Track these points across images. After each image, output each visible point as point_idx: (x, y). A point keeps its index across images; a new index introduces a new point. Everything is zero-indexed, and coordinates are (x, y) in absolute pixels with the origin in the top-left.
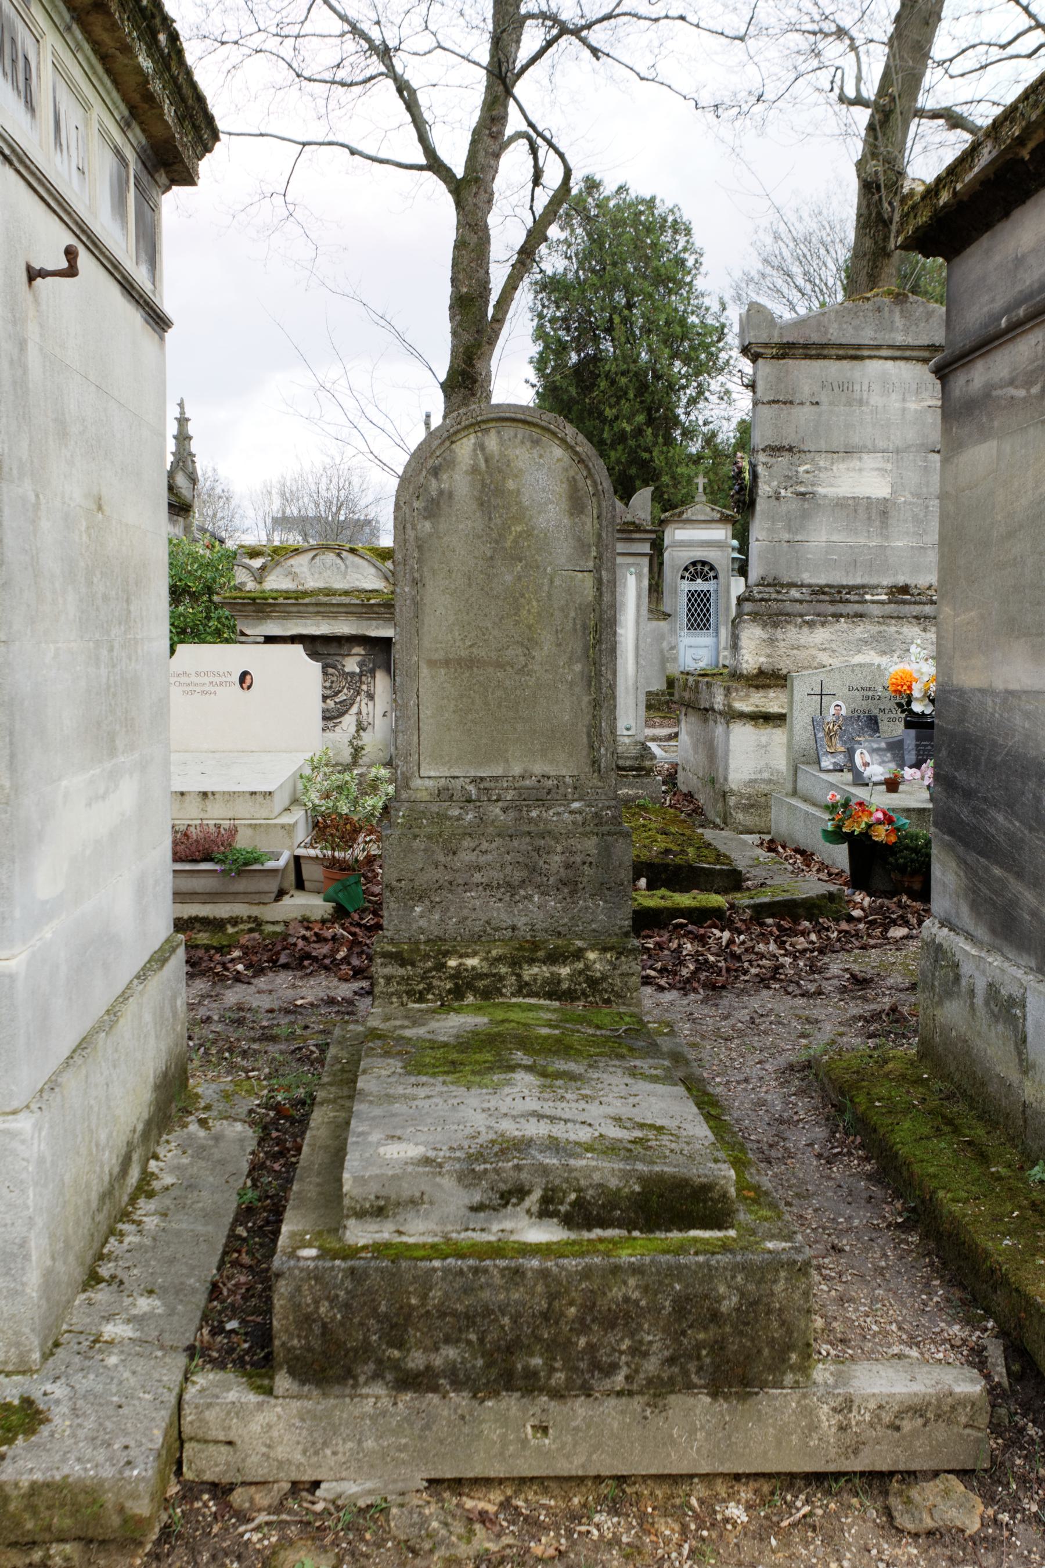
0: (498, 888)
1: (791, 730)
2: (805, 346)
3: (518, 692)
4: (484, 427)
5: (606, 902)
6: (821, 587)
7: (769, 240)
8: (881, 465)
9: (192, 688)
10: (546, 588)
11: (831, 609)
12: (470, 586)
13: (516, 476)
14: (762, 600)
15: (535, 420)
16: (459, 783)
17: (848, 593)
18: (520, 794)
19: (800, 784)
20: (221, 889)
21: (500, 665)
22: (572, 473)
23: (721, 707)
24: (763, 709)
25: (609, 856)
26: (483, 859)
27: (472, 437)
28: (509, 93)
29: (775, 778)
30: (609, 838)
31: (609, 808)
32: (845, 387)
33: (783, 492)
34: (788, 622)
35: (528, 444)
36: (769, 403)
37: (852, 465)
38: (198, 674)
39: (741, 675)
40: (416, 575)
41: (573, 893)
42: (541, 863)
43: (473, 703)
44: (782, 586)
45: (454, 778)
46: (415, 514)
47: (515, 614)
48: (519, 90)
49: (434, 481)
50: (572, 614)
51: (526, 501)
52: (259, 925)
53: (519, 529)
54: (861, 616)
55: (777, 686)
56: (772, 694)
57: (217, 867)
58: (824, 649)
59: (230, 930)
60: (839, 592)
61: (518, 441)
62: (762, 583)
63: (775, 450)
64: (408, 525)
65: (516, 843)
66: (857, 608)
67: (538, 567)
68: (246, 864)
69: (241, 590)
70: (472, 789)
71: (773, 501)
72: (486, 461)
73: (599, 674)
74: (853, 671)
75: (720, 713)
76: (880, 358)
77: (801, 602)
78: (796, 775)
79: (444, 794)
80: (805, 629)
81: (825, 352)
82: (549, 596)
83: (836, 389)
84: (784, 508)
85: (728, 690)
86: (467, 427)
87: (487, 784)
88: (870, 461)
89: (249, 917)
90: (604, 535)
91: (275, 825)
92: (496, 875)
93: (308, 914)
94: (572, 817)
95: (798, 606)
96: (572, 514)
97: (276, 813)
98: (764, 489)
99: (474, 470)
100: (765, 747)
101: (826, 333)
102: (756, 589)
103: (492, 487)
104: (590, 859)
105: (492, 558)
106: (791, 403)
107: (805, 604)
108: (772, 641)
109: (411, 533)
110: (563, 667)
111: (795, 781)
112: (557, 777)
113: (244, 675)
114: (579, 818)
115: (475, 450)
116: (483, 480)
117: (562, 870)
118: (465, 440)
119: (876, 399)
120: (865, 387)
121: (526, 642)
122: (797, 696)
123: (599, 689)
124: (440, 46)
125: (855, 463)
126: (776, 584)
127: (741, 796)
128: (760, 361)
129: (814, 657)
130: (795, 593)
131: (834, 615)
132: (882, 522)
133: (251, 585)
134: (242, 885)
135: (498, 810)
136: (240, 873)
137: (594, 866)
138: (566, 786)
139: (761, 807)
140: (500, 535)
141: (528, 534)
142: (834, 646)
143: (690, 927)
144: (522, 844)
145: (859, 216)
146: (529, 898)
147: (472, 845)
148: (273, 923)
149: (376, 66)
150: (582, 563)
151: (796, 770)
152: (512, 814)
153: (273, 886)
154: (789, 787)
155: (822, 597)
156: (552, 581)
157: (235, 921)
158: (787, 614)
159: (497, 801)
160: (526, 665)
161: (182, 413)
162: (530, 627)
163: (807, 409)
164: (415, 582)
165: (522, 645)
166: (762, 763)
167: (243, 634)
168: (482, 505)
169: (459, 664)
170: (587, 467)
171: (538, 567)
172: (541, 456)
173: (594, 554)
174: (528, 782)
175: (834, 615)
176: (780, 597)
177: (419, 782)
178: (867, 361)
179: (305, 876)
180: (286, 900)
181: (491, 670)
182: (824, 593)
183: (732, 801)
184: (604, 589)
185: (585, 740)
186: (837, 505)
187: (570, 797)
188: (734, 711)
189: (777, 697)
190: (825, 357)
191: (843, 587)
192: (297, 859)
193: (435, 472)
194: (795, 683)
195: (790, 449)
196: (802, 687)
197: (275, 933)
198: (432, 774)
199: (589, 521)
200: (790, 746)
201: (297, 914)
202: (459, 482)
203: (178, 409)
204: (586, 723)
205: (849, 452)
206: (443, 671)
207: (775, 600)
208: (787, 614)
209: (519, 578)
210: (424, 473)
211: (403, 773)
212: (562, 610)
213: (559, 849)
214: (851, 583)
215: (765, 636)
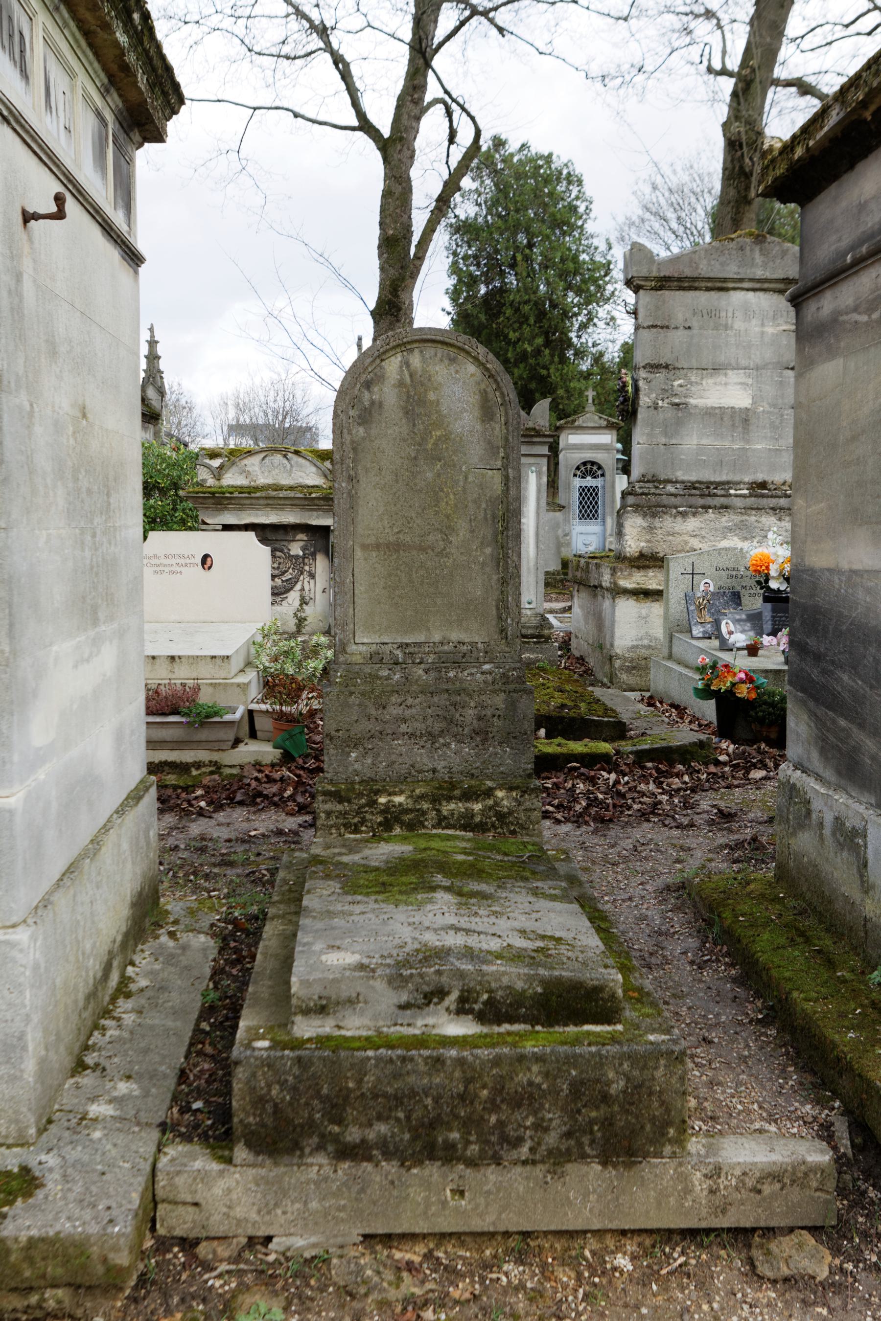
0: (421, 737)
2: (679, 279)
3: (438, 572)
4: (409, 347)
5: (512, 748)
6: (693, 483)
7: (648, 189)
8: (744, 380)
9: (161, 568)
10: (461, 484)
11: (701, 501)
12: (397, 481)
13: (436, 389)
14: (643, 494)
15: (452, 341)
16: (388, 648)
17: (716, 488)
18: (440, 658)
19: (675, 649)
20: (187, 738)
21: (422, 549)
22: (483, 386)
23: (608, 585)
24: (644, 586)
26: (408, 712)
27: (399, 356)
28: (428, 65)
29: (653, 644)
31: (514, 669)
32: (712, 314)
33: (660, 403)
35: (446, 362)
36: (649, 327)
37: (718, 380)
38: (166, 557)
39: (625, 558)
40: (352, 473)
41: (484, 740)
42: (457, 716)
43: (400, 581)
44: (660, 482)
45: (383, 644)
47: (436, 506)
49: (366, 393)
53: (438, 433)
54: (727, 507)
55: (655, 567)
56: (651, 573)
57: (183, 720)
58: (695, 536)
59: (194, 772)
60: (708, 488)
61: (437, 359)
62: (643, 480)
63: (654, 367)
64: (345, 431)
65: (436, 699)
66: (723, 500)
67: (454, 466)
68: (207, 717)
70: (399, 654)
72: (411, 376)
73: (506, 556)
74: (719, 554)
75: (607, 590)
76: (742, 289)
77: (675, 495)
78: (671, 641)
79: (376, 658)
80: (679, 519)
81: (696, 284)
82: (464, 490)
85: (614, 571)
86: (394, 348)
87: (411, 649)
88: (734, 377)
89: (210, 762)
91: (232, 684)
92: (419, 726)
93: (260, 758)
95: (673, 499)
96: (483, 421)
97: (233, 674)
98: (644, 400)
99: (401, 384)
100: (644, 619)
101: (697, 268)
102: (637, 485)
104: (498, 713)
105: (415, 458)
106: (667, 327)
107: (679, 498)
108: (651, 529)
109: (347, 438)
110: (476, 550)
111: (671, 647)
112: (471, 643)
113: (205, 557)
114: (489, 678)
115: (401, 367)
116: (408, 392)
117: (475, 721)
119: (739, 325)
120: (730, 314)
121: (444, 529)
122: (672, 576)
123: (506, 569)
125: (721, 379)
126: (654, 480)
127: (625, 659)
128: (641, 292)
129: (686, 543)
130: (670, 488)
131: (703, 507)
132: (744, 428)
133: (211, 482)
134: (204, 734)
135: (421, 672)
136: (202, 724)
137: (502, 718)
138: (479, 651)
139: (641, 669)
140: (422, 439)
141: (446, 438)
142: (703, 533)
143: (582, 770)
144: (441, 700)
145: (725, 169)
146: (447, 745)
148: (230, 767)
149: (316, 42)
152: (433, 675)
153: (231, 735)
154: (665, 651)
155: (694, 492)
156: (466, 478)
157: (198, 765)
158: (664, 506)
159: (420, 663)
160: (445, 549)
161: (152, 336)
162: (448, 516)
163: (681, 332)
164: (351, 479)
165: (441, 532)
166: (643, 632)
167: (204, 523)
168: (407, 413)
170: (496, 381)
172: (457, 372)
173: (502, 455)
174: (446, 648)
175: (703, 507)
176: (658, 491)
177: (354, 647)
178: (732, 292)
180: (242, 747)
181: (414, 552)
182: (695, 488)
183: (617, 663)
184: (511, 484)
185: (494, 612)
186: (706, 413)
187: (481, 660)
189: (655, 576)
190: (696, 289)
191: (712, 483)
192: (251, 713)
193: (368, 385)
194: (671, 564)
195: (667, 367)
196: (676, 567)
197: (231, 775)
198: (365, 641)
201: (251, 760)
202: (388, 394)
204: (495, 597)
205: (717, 369)
206: (374, 554)
207: (653, 494)
208: (664, 506)
209: (439, 475)
210: (358, 386)
211: (340, 640)
213: (473, 704)
215: (645, 525)
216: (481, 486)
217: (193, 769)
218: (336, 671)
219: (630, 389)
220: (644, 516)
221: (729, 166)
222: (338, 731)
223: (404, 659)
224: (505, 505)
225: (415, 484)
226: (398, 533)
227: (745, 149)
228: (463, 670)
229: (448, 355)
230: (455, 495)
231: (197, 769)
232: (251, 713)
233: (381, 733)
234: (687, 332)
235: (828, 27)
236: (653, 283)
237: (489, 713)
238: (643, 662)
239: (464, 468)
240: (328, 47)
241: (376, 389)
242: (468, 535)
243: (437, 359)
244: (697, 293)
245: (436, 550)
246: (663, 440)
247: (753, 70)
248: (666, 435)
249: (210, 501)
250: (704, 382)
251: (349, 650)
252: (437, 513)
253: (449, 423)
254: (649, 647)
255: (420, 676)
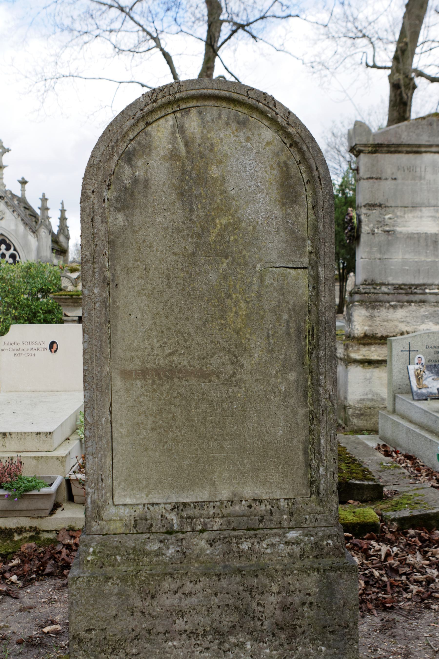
0: (204, 636)
1: (390, 372)
2: (388, 146)
3: (225, 405)
4: (183, 106)
5: (329, 647)
6: (400, 285)
7: (330, 135)
8: (433, 214)
9: (20, 352)
10: (255, 287)
11: (406, 298)
12: (169, 285)
13: (221, 162)
14: (365, 293)
15: (241, 97)
16: (160, 510)
17: (416, 289)
18: (229, 523)
19: (398, 407)
20: (10, 508)
21: (204, 375)
22: (283, 158)
23: (342, 356)
24: (368, 358)
25: (332, 594)
26: (186, 603)
27: (170, 118)
28: (215, 54)
29: (375, 398)
30: (332, 574)
31: (330, 537)
32: (411, 169)
33: (376, 230)
34: (381, 306)
35: (234, 126)
36: (368, 179)
37: (416, 214)
38: (24, 343)
39: (354, 338)
40: (108, 274)
41: (291, 638)
42: (254, 604)
43: (174, 419)
44: (377, 285)
45: (153, 504)
46: (106, 205)
47: (221, 317)
48: (219, 53)
49: (127, 168)
50: (285, 316)
51: (231, 188)
52: (38, 533)
53: (224, 221)
54: (424, 302)
55: (376, 344)
56: (373, 348)
57: (6, 493)
58: (403, 322)
59: (17, 537)
60: (410, 288)
61: (222, 122)
62: (365, 283)
63: (371, 206)
64: (98, 218)
65: (224, 583)
66: (421, 297)
67: (246, 264)
68: (26, 491)
69: (65, 291)
70: (173, 517)
71: (371, 236)
72: (187, 145)
73: (316, 384)
74: (428, 336)
75: (341, 359)
76: (431, 152)
77: (388, 294)
78: (394, 400)
79: (141, 525)
80: (391, 310)
81: (400, 149)
82: (259, 295)
83: (406, 171)
84: (377, 239)
85: (347, 347)
86: (163, 106)
87: (190, 512)
88: (426, 212)
89: (31, 527)
90: (321, 227)
91: (52, 457)
92: (202, 621)
93: (73, 524)
94: (288, 549)
95: (386, 297)
96: (284, 204)
97: (56, 445)
98: (365, 229)
99: (173, 155)
100: (369, 380)
101: (400, 138)
102: (361, 287)
103: (194, 174)
104: (310, 599)
105: (194, 254)
106: (380, 179)
107: (391, 296)
108: (372, 317)
109: (101, 228)
110: (276, 376)
111: (394, 404)
112: (270, 501)
113: (53, 343)
114: (296, 549)
115: (173, 133)
116: (183, 167)
117: (278, 612)
118: (162, 121)
119: (429, 176)
120: (423, 169)
121: (233, 349)
122: (394, 352)
123: (317, 401)
124: (182, 31)
125: (418, 213)
126: (373, 284)
127: (356, 409)
128: (362, 155)
129: (396, 326)
130: (384, 289)
131: (408, 302)
132: (434, 247)
133: (70, 288)
134: (24, 505)
135: (203, 543)
136: (22, 497)
137: (315, 607)
138: (281, 512)
139: (367, 415)
140: (203, 228)
141: (235, 227)
142: (408, 319)
143: (355, 541)
144: (231, 583)
145: (391, 101)
146: (240, 645)
147: (174, 586)
148: (48, 532)
149: (152, 43)
150: (296, 259)
151: (395, 397)
152: (220, 547)
153: (49, 505)
154: (390, 408)
155: (401, 291)
156: (262, 280)
157: (20, 530)
158: (380, 301)
159: (202, 531)
160: (234, 375)
161: (63, 207)
162: (238, 331)
163: (389, 182)
164: (106, 282)
165: (229, 352)
166: (368, 389)
167: (66, 315)
168: (182, 194)
169: (158, 374)
170: (300, 151)
171: (246, 264)
172: (248, 139)
173: (309, 248)
174: (237, 508)
175: (408, 302)
176: (376, 291)
177: (113, 510)
178: (424, 155)
179: (74, 493)
180: (59, 514)
181: (193, 380)
182: (401, 289)
183: (350, 412)
184: (322, 288)
185: (301, 458)
186: (408, 237)
187: (285, 524)
188: (351, 359)
189: (376, 350)
190: (399, 152)
191: (413, 285)
192: (68, 482)
193: (129, 157)
194: (393, 344)
195: (380, 206)
196: (398, 345)
197: (49, 539)
198: (128, 501)
199: (303, 212)
200: (390, 382)
201: (65, 525)
202: (156, 169)
203: (61, 205)
204: (302, 438)
205: (414, 207)
206: (139, 383)
207: (373, 293)
208: (380, 301)
209: (225, 277)
210: (115, 158)
211: (93, 502)
212: (273, 311)
213: (275, 588)
214: (417, 282)
215: (367, 314)
216: (282, 291)
217: (15, 534)
218: (88, 546)
219: (355, 221)
220: (367, 308)
221: (393, 98)
222: (89, 631)
223: (181, 525)
224: (313, 316)
225: (194, 289)
226: (171, 354)
227: (403, 89)
228: (261, 540)
229: (236, 116)
230: (247, 302)
231: (19, 534)
232: (68, 482)
233: (149, 632)
234: (394, 182)
235: (430, 43)
236: (370, 149)
237: (297, 599)
238: (368, 411)
239: (258, 267)
240: (158, 45)
241: (139, 163)
242: (265, 356)
243: (222, 122)
244: (400, 155)
245: (223, 377)
246: (379, 256)
247: (406, 44)
248: (380, 252)
249: (70, 300)
250: (406, 216)
251: (105, 515)
252: (223, 327)
253: (238, 207)
254: (372, 400)
255: (202, 550)
